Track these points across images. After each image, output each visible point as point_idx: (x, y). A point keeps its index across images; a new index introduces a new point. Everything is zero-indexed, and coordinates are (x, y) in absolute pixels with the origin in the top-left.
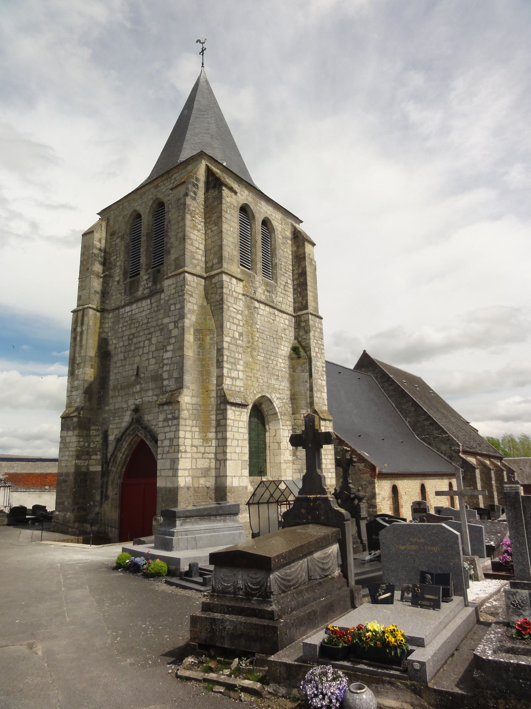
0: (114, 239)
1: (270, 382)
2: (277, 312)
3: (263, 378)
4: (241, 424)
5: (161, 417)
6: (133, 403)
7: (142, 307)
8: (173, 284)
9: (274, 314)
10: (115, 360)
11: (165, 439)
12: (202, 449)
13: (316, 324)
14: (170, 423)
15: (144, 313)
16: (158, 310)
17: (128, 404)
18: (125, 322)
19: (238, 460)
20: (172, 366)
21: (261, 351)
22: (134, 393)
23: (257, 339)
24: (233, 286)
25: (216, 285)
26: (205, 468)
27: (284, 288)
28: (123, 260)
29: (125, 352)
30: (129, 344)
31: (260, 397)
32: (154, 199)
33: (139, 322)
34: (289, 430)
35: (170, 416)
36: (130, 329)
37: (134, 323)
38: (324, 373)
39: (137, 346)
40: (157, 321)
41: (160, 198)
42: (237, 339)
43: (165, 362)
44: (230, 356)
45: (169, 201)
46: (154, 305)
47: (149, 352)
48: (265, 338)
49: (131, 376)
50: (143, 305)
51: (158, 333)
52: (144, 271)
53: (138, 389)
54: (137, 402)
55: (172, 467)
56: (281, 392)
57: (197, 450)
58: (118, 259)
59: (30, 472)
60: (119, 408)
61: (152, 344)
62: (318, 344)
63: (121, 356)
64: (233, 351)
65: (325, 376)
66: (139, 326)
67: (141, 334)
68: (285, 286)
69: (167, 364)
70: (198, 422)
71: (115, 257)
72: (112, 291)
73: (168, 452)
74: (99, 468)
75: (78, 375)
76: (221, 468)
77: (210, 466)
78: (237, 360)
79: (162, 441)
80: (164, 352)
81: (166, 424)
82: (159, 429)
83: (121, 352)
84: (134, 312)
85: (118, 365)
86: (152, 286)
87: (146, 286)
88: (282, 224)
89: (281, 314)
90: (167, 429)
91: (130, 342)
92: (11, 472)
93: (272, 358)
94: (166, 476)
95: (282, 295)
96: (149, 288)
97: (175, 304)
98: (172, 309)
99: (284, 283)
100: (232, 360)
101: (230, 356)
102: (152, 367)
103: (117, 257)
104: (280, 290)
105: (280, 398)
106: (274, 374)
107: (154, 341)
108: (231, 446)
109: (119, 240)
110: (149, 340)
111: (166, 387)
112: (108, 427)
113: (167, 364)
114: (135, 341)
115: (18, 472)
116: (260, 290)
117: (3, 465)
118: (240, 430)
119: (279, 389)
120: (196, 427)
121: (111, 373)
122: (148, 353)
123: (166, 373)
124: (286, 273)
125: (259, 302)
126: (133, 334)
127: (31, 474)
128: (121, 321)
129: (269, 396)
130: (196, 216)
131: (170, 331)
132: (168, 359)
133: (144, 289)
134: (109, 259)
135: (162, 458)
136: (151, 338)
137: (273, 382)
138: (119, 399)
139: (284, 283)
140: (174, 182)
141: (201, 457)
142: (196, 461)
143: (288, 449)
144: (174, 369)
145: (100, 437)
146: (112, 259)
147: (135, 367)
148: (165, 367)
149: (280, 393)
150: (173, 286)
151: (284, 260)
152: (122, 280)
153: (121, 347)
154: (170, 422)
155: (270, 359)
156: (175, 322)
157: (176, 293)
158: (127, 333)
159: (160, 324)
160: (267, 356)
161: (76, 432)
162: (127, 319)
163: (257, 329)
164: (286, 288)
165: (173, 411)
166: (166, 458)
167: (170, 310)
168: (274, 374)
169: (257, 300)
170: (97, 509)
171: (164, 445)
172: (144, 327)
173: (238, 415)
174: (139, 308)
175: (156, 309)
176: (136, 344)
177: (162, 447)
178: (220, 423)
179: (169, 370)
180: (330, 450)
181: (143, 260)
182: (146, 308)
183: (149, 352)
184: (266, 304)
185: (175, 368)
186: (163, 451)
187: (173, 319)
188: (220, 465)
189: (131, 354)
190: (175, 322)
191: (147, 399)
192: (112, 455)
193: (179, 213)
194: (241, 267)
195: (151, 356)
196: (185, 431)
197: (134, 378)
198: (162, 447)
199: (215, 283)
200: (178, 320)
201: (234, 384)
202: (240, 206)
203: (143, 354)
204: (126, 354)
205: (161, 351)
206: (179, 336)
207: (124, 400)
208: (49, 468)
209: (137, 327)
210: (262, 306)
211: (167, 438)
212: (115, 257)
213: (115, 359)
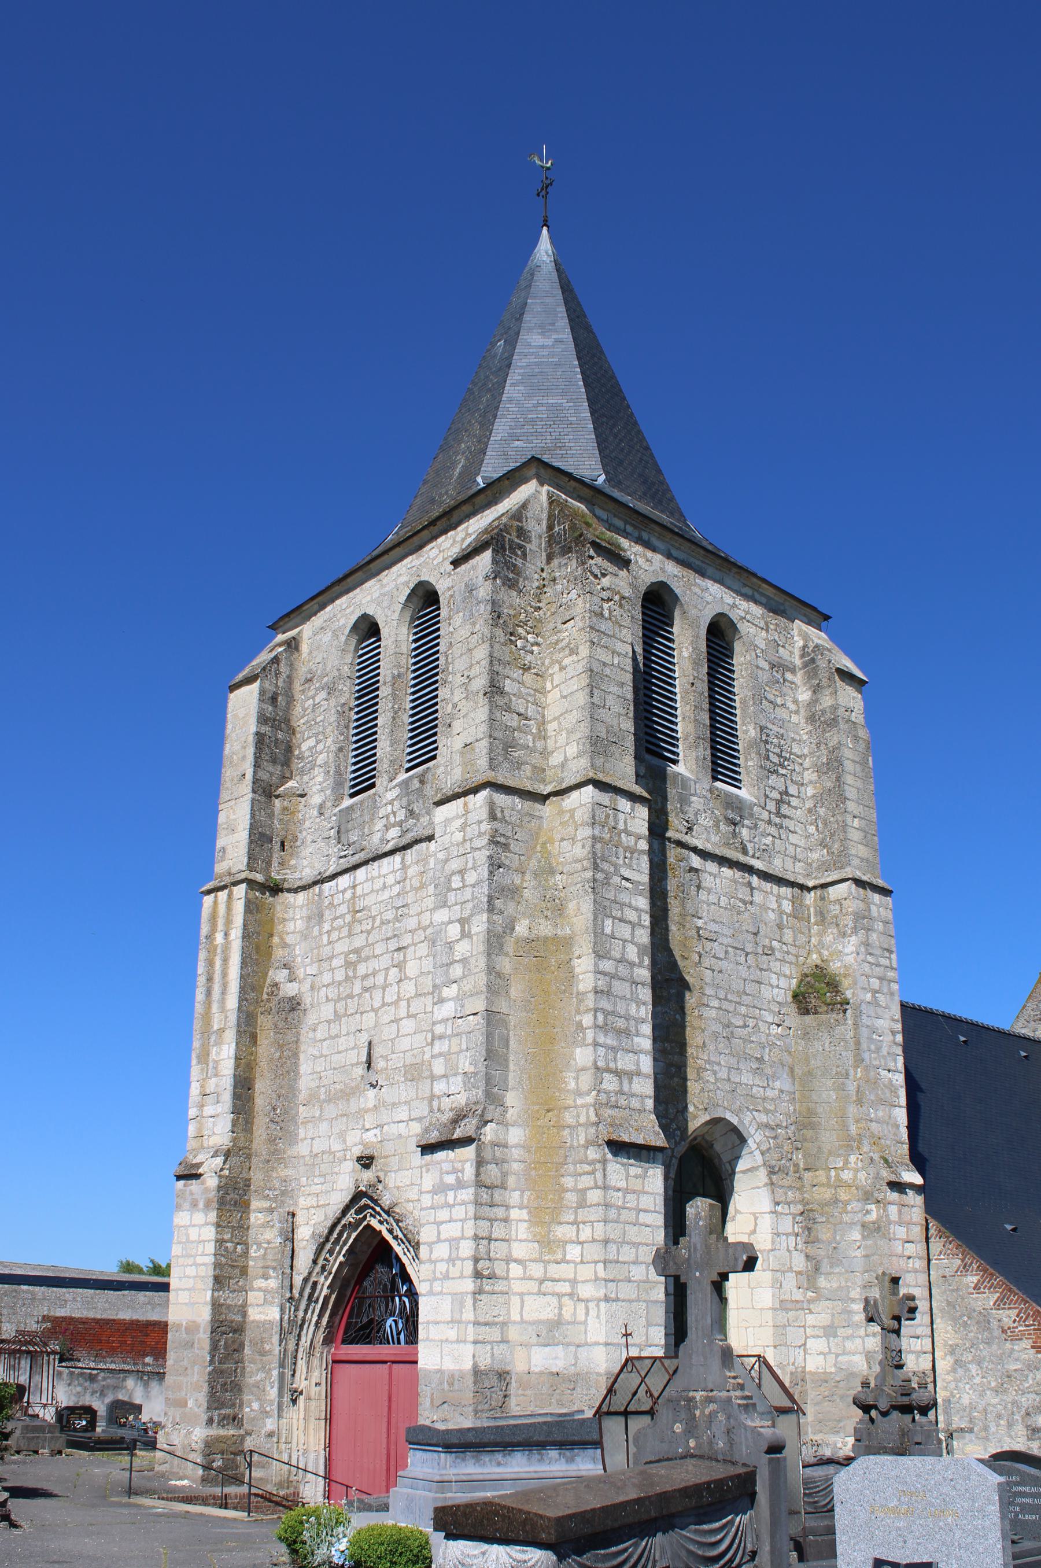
0: (311, 694)
1: (737, 1080)
2: (755, 880)
3: (716, 1068)
4: (646, 1202)
5: (428, 1182)
6: (357, 1140)
7: (380, 876)
8: (457, 817)
9: (749, 884)
10: (310, 1022)
11: (439, 1241)
12: (536, 1270)
13: (873, 908)
14: (450, 1199)
15: (386, 895)
16: (422, 886)
17: (345, 1141)
18: (336, 918)
19: (638, 1300)
20: (455, 1041)
21: (709, 991)
22: (361, 1113)
23: (696, 958)
24: (621, 816)
25: (572, 816)
26: (548, 1321)
27: (778, 809)
28: (333, 748)
29: (339, 999)
30: (347, 978)
31: (707, 1123)
32: (412, 586)
33: (374, 918)
34: (794, 1216)
35: (450, 1179)
36: (350, 935)
37: (360, 922)
38: (899, 1050)
39: (368, 983)
40: (418, 914)
41: (428, 582)
42: (632, 965)
43: (439, 1029)
44: (613, 1013)
45: (449, 589)
46: (411, 872)
47: (399, 999)
48: (722, 956)
49: (352, 1065)
50: (384, 871)
51: (423, 949)
52: (386, 777)
53: (371, 1104)
54: (370, 1137)
55: (457, 1317)
56: (772, 1108)
57: (525, 1272)
58: (320, 747)
59: (104, 1316)
60: (323, 1152)
61: (406, 978)
62: (878, 965)
63: (327, 1011)
64: (623, 998)
65: (900, 1060)
66: (373, 928)
67: (377, 952)
68: (779, 802)
69: (441, 1037)
70: (527, 1193)
71: (311, 742)
72: (304, 833)
73: (446, 1277)
74: (273, 1314)
75: (216, 1062)
76: (589, 1322)
77: (560, 1314)
78: (632, 1022)
79: (430, 1245)
80: (434, 1004)
81: (439, 1199)
82: (423, 1213)
83: (328, 1000)
84: (359, 891)
85: (319, 1035)
86: (406, 821)
87: (392, 819)
88: (767, 631)
89: (768, 886)
90: (443, 1215)
91: (351, 974)
92: (58, 1314)
93: (743, 1010)
94: (442, 1341)
95: (773, 830)
96: (400, 824)
97: (462, 872)
98: (454, 886)
99: (775, 795)
100: (621, 1023)
101: (613, 1013)
102: (405, 1044)
103: (318, 742)
104: (765, 815)
105: (767, 1126)
106: (748, 1057)
107: (412, 968)
108: (617, 1262)
109: (323, 695)
110: (400, 966)
111: (439, 1097)
112: (296, 1204)
113: (441, 1037)
114: (362, 969)
115: (76, 1315)
116: (705, 821)
117: (40, 1296)
118: (644, 1218)
119: (764, 1099)
120: (521, 1208)
121: (302, 1056)
122: (396, 1003)
123: (441, 1060)
124: (783, 767)
125: (704, 855)
126: (357, 951)
127: (108, 1322)
128: (328, 915)
129: (734, 1120)
130: (520, 630)
131: (450, 946)
132: (445, 1021)
133: (387, 828)
134: (299, 747)
135: (431, 1293)
136: (405, 961)
137: (746, 1078)
138: (324, 1126)
139: (775, 795)
140: (463, 540)
141: (536, 1290)
142: (522, 1302)
143: (791, 1270)
144: (461, 1051)
145: (275, 1231)
146: (304, 747)
147: (364, 1038)
148: (437, 1043)
149: (767, 1112)
150: (458, 823)
151: (775, 728)
152: (329, 804)
153: (327, 986)
154: (451, 1196)
155: (736, 1013)
156: (462, 921)
157: (465, 840)
158: (341, 947)
159: (428, 923)
160: (725, 1005)
161: (213, 1216)
162: (343, 909)
163: (698, 929)
164: (785, 810)
165: (458, 1165)
166: (441, 1293)
167: (450, 889)
168: (748, 1057)
169: (695, 850)
170: (270, 1424)
171: (434, 1257)
172: (388, 931)
173: (636, 1177)
174: (373, 878)
175: (416, 883)
176: (365, 977)
177: (431, 1261)
178: (585, 1200)
179: (449, 1053)
180: (916, 1271)
181: (384, 748)
182: (390, 880)
183: (399, 999)
184: (723, 861)
185: (464, 1047)
186: (434, 1272)
187: (456, 912)
188: (587, 1314)
189: (352, 1005)
190: (462, 921)
191: (392, 1130)
192: (306, 1280)
193: (474, 624)
194: (648, 757)
195: (403, 1013)
196: (490, 1220)
197: (360, 1071)
198: (431, 1261)
199: (572, 812)
200: (472, 915)
201: (626, 1088)
202: (643, 589)
203: (384, 1005)
204: (340, 1006)
205: (429, 1000)
206: (473, 960)
207: (335, 1130)
208: (153, 1309)
209: (369, 932)
210: (711, 867)
211: (442, 1237)
212: (311, 742)
213: (311, 1019)
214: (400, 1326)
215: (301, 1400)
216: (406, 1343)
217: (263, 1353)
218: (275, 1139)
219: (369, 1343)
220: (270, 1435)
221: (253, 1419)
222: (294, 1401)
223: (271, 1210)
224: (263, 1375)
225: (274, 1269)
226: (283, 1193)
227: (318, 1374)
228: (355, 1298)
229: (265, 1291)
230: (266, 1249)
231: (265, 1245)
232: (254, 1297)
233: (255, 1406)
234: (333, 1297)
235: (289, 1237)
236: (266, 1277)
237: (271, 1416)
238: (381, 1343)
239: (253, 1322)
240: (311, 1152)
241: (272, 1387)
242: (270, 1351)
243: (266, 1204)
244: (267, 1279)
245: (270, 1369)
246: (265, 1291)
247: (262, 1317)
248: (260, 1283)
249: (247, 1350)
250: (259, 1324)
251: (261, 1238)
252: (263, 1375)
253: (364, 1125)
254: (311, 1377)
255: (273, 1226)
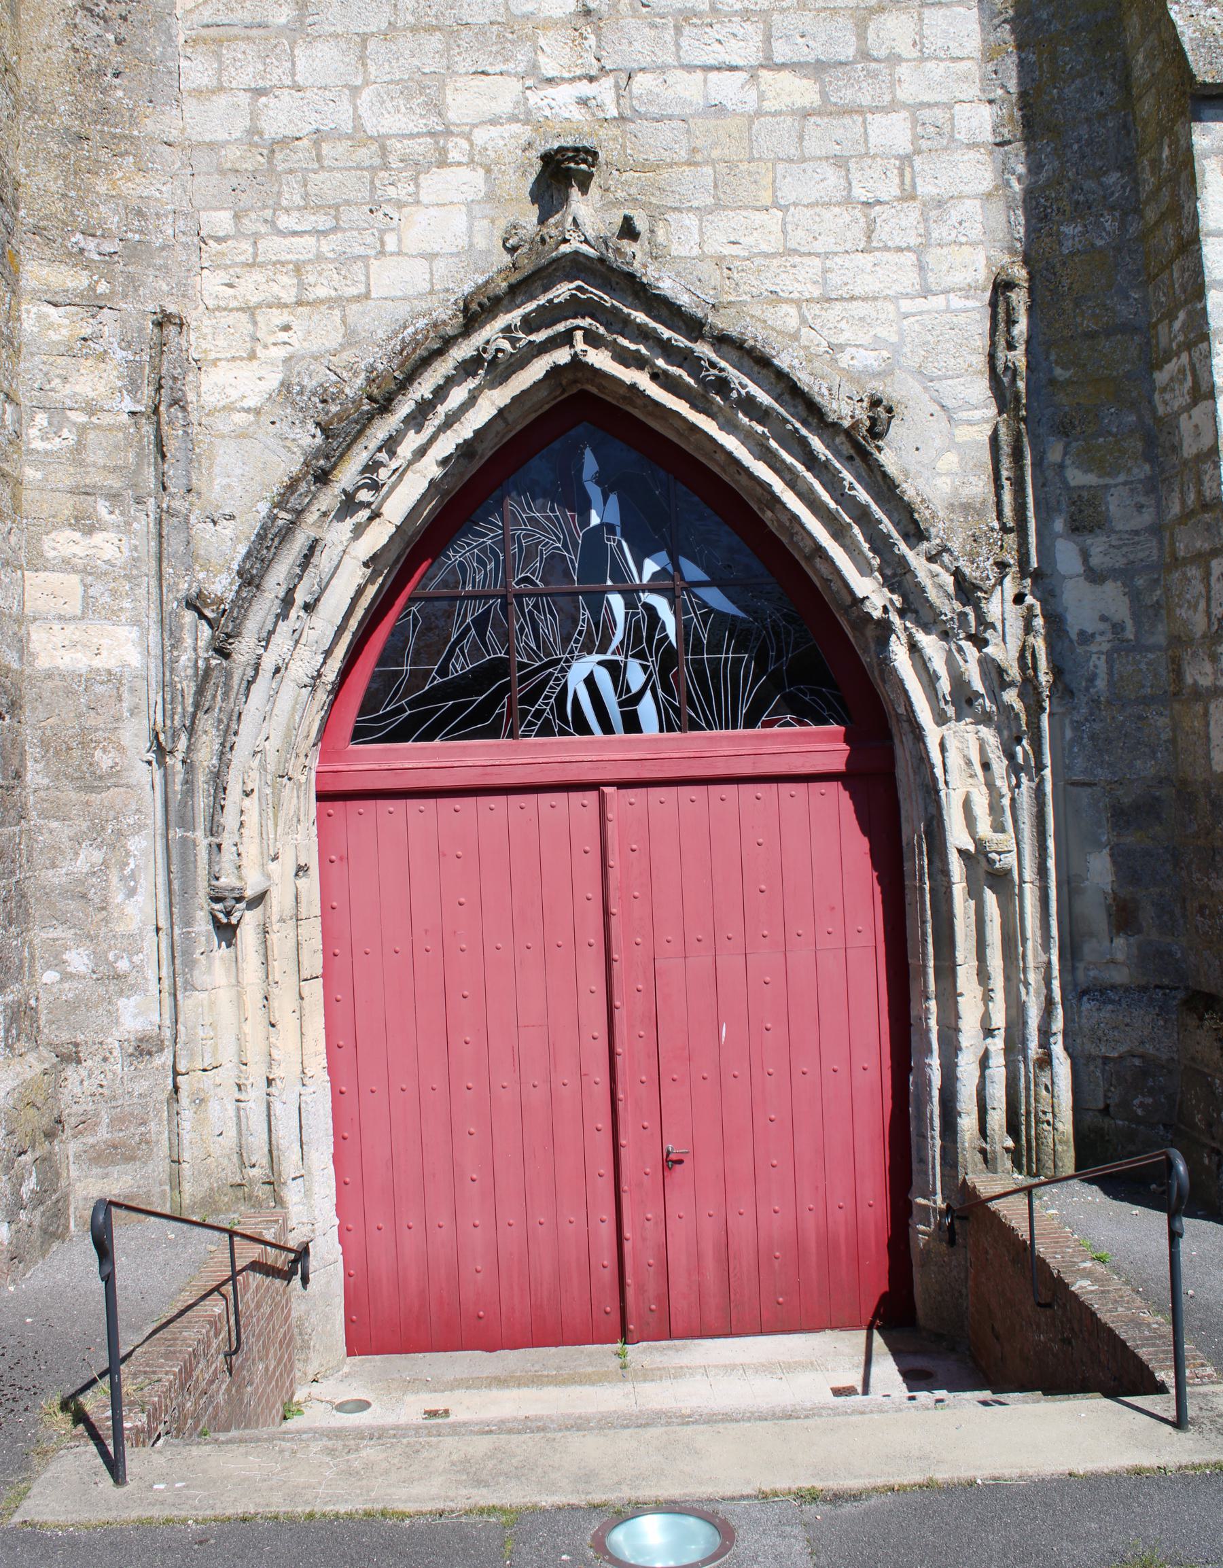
214: (636, 677)
215: (249, 924)
216: (667, 725)
217: (92, 781)
218: (100, 72)
219: (492, 732)
220: (143, 1048)
221: (73, 1006)
222: (226, 931)
223: (95, 304)
224: (98, 856)
225: (114, 497)
226: (136, 252)
227: (303, 841)
228: (412, 600)
229: (84, 571)
230: (82, 430)
231: (80, 418)
232: (46, 590)
233: (78, 960)
234: (371, 591)
235: (163, 400)
236: (86, 524)
237: (134, 989)
238: (546, 730)
239: (50, 676)
240: (254, 131)
241: (131, 893)
242: (115, 773)
243: (76, 280)
244: (89, 531)
245: (119, 834)
246: (84, 571)
247: (77, 661)
248: (63, 543)
249: (35, 775)
250: (73, 685)
251: (62, 392)
252: (98, 856)
253: (534, 67)
254: (274, 843)
255: (102, 357)
